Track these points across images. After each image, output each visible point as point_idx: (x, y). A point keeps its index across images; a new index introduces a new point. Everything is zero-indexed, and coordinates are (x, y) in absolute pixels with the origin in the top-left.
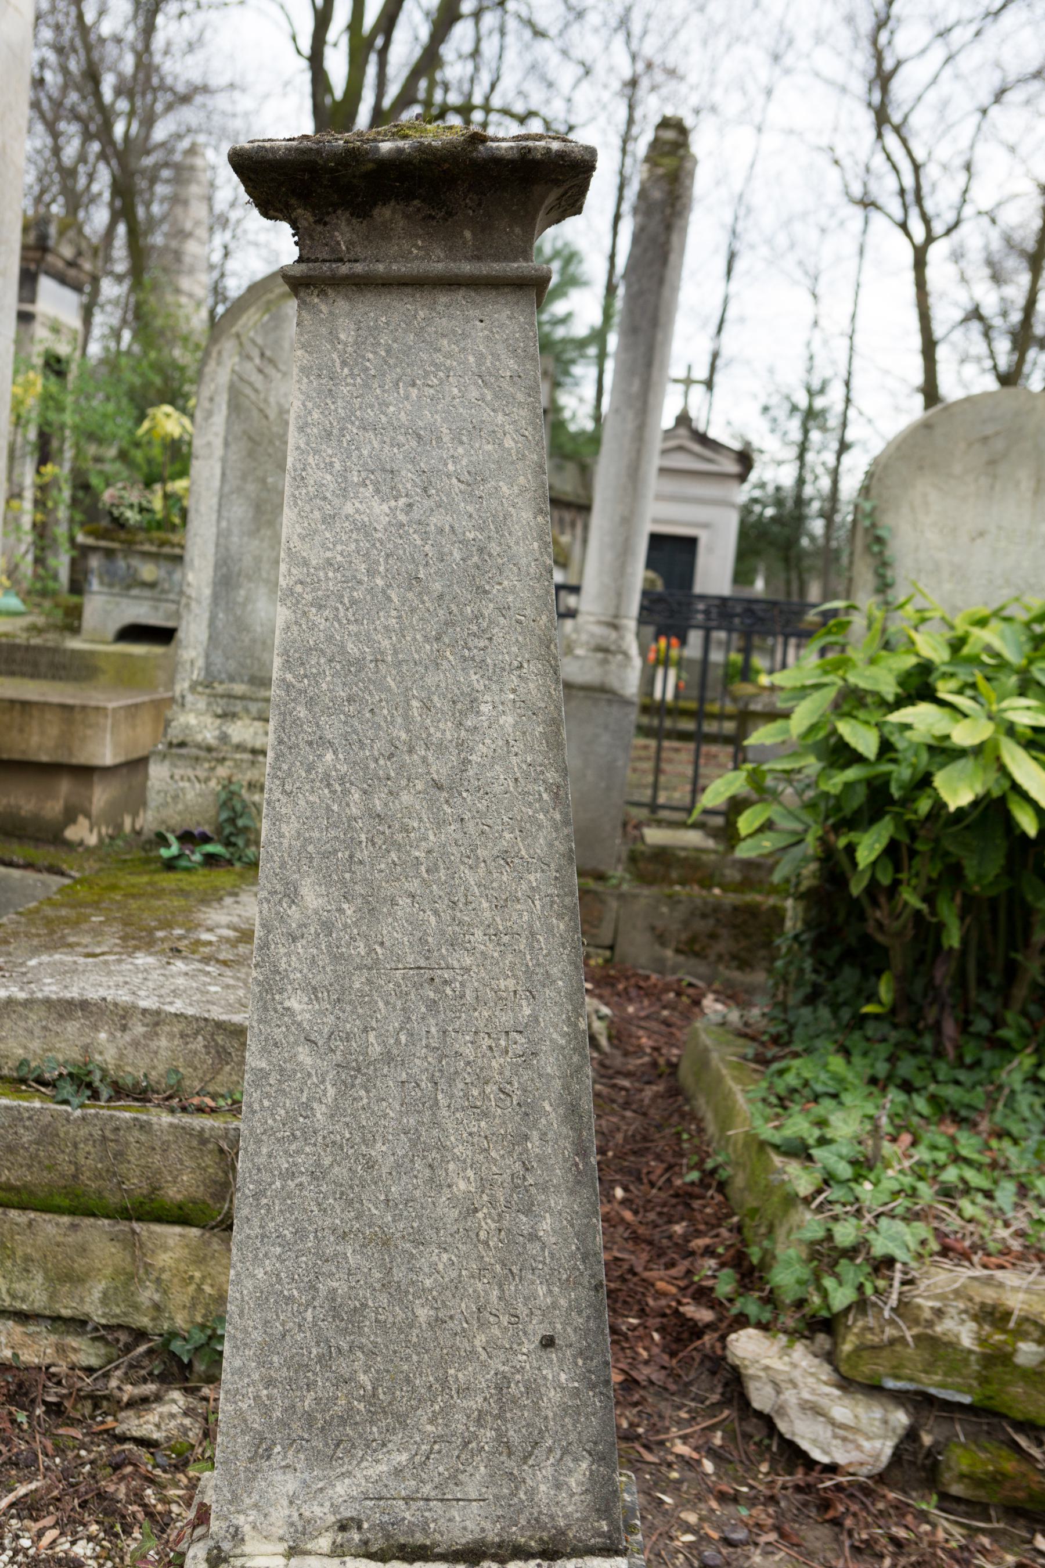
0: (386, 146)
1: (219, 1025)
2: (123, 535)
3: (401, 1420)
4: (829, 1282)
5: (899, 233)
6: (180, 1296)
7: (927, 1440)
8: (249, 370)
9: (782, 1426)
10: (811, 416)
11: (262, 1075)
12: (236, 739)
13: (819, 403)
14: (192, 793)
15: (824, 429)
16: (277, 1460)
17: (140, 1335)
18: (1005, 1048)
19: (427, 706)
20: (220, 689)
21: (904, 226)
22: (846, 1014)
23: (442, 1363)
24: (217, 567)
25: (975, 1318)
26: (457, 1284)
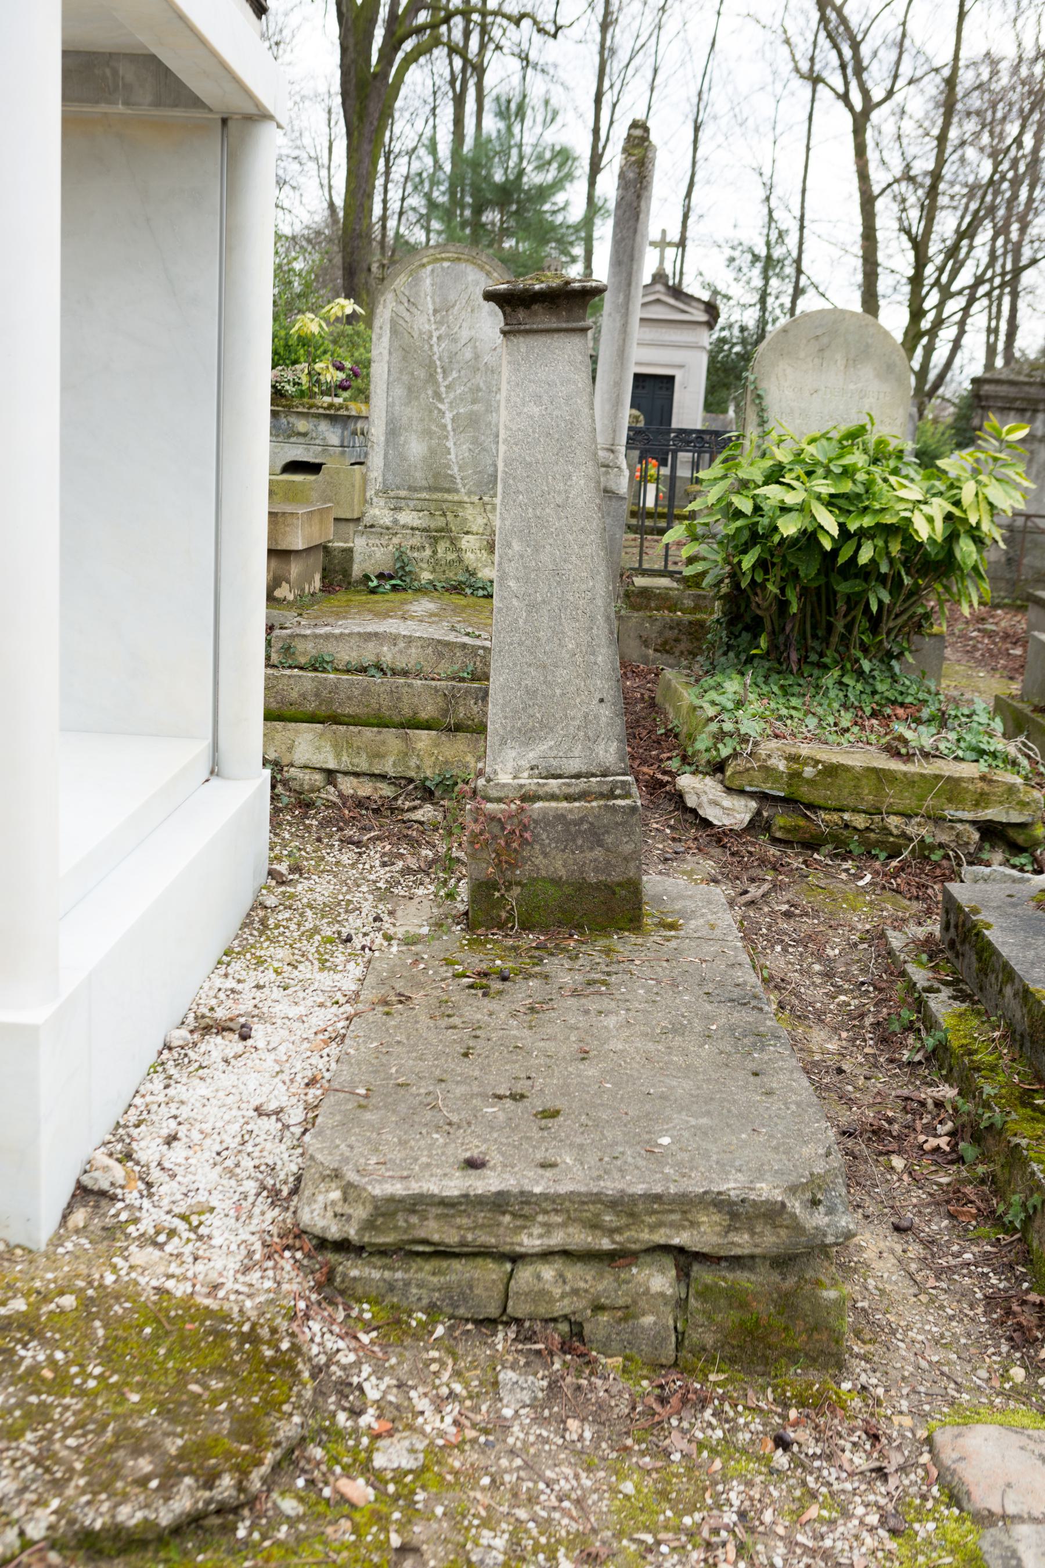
0: (537, 287)
1: (439, 641)
2: (284, 402)
3: (551, 729)
4: (720, 746)
5: (840, 105)
6: (428, 762)
7: (765, 814)
8: (401, 310)
9: (701, 812)
10: (769, 264)
11: (500, 609)
12: (402, 522)
13: (777, 253)
14: (379, 553)
15: (782, 278)
16: (509, 745)
17: (411, 780)
18: (826, 668)
19: (554, 478)
20: (392, 494)
21: (845, 98)
22: (743, 657)
23: (565, 709)
24: (387, 424)
25: (786, 759)
26: (570, 681)
